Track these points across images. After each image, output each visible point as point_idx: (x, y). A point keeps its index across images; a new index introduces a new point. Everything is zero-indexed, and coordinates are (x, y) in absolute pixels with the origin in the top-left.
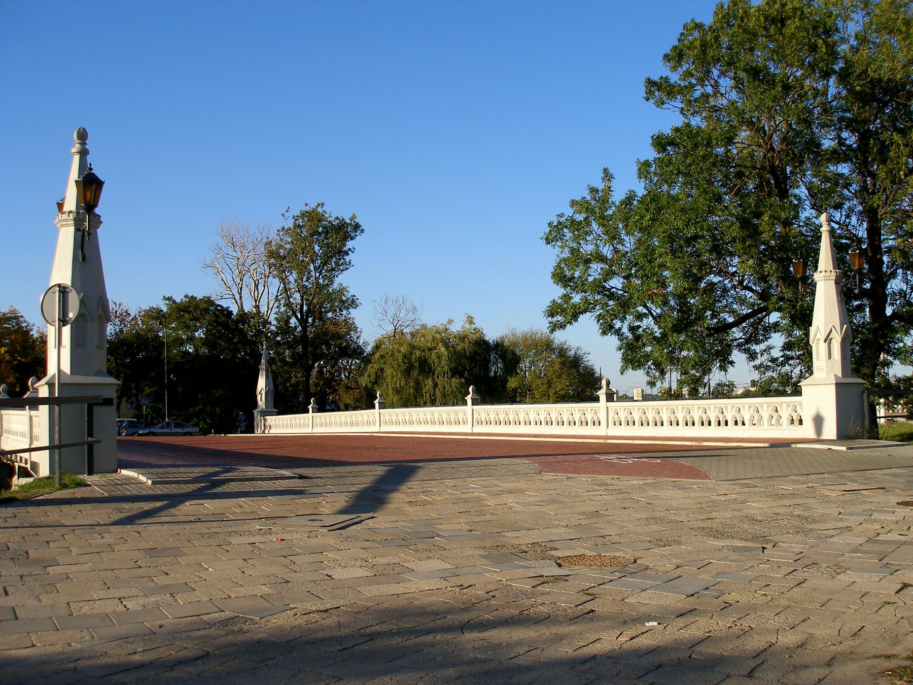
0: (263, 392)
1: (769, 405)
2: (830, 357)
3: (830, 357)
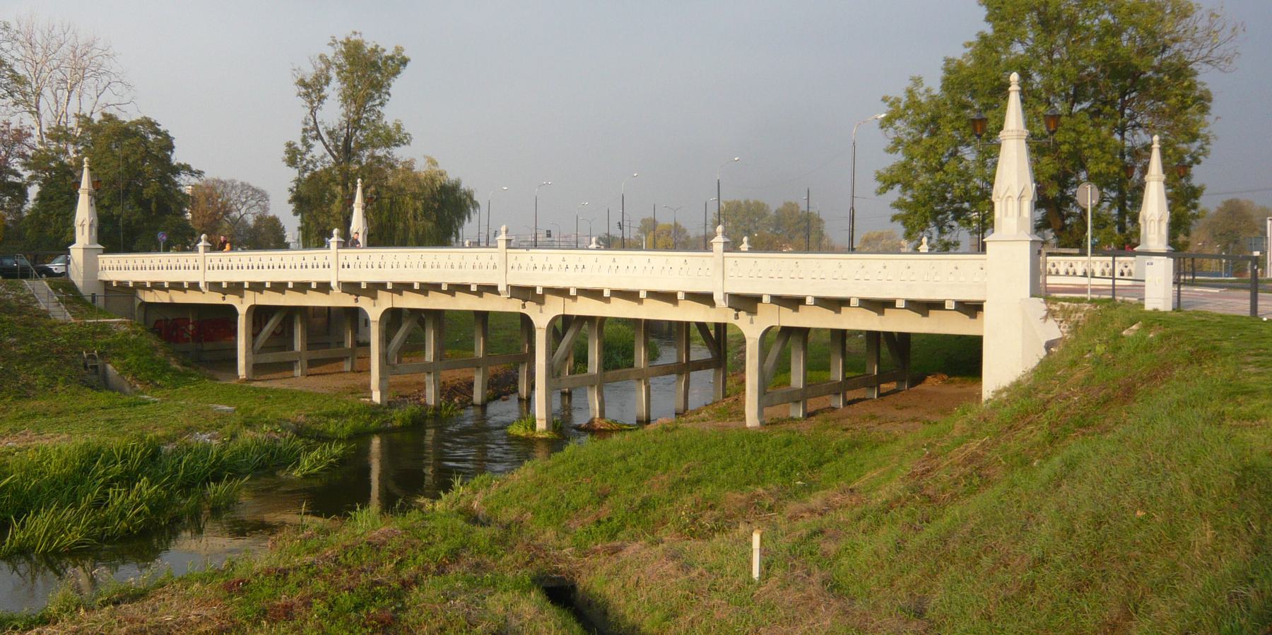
0: (87, 224)
1: (1101, 262)
2: (83, 234)
3: (83, 234)
